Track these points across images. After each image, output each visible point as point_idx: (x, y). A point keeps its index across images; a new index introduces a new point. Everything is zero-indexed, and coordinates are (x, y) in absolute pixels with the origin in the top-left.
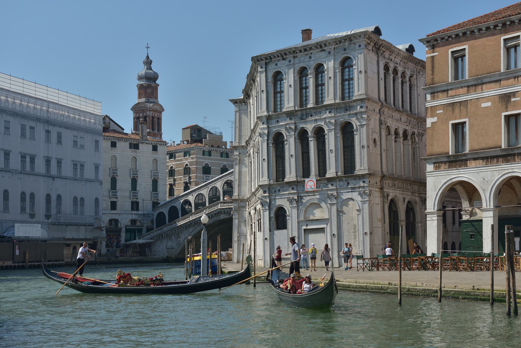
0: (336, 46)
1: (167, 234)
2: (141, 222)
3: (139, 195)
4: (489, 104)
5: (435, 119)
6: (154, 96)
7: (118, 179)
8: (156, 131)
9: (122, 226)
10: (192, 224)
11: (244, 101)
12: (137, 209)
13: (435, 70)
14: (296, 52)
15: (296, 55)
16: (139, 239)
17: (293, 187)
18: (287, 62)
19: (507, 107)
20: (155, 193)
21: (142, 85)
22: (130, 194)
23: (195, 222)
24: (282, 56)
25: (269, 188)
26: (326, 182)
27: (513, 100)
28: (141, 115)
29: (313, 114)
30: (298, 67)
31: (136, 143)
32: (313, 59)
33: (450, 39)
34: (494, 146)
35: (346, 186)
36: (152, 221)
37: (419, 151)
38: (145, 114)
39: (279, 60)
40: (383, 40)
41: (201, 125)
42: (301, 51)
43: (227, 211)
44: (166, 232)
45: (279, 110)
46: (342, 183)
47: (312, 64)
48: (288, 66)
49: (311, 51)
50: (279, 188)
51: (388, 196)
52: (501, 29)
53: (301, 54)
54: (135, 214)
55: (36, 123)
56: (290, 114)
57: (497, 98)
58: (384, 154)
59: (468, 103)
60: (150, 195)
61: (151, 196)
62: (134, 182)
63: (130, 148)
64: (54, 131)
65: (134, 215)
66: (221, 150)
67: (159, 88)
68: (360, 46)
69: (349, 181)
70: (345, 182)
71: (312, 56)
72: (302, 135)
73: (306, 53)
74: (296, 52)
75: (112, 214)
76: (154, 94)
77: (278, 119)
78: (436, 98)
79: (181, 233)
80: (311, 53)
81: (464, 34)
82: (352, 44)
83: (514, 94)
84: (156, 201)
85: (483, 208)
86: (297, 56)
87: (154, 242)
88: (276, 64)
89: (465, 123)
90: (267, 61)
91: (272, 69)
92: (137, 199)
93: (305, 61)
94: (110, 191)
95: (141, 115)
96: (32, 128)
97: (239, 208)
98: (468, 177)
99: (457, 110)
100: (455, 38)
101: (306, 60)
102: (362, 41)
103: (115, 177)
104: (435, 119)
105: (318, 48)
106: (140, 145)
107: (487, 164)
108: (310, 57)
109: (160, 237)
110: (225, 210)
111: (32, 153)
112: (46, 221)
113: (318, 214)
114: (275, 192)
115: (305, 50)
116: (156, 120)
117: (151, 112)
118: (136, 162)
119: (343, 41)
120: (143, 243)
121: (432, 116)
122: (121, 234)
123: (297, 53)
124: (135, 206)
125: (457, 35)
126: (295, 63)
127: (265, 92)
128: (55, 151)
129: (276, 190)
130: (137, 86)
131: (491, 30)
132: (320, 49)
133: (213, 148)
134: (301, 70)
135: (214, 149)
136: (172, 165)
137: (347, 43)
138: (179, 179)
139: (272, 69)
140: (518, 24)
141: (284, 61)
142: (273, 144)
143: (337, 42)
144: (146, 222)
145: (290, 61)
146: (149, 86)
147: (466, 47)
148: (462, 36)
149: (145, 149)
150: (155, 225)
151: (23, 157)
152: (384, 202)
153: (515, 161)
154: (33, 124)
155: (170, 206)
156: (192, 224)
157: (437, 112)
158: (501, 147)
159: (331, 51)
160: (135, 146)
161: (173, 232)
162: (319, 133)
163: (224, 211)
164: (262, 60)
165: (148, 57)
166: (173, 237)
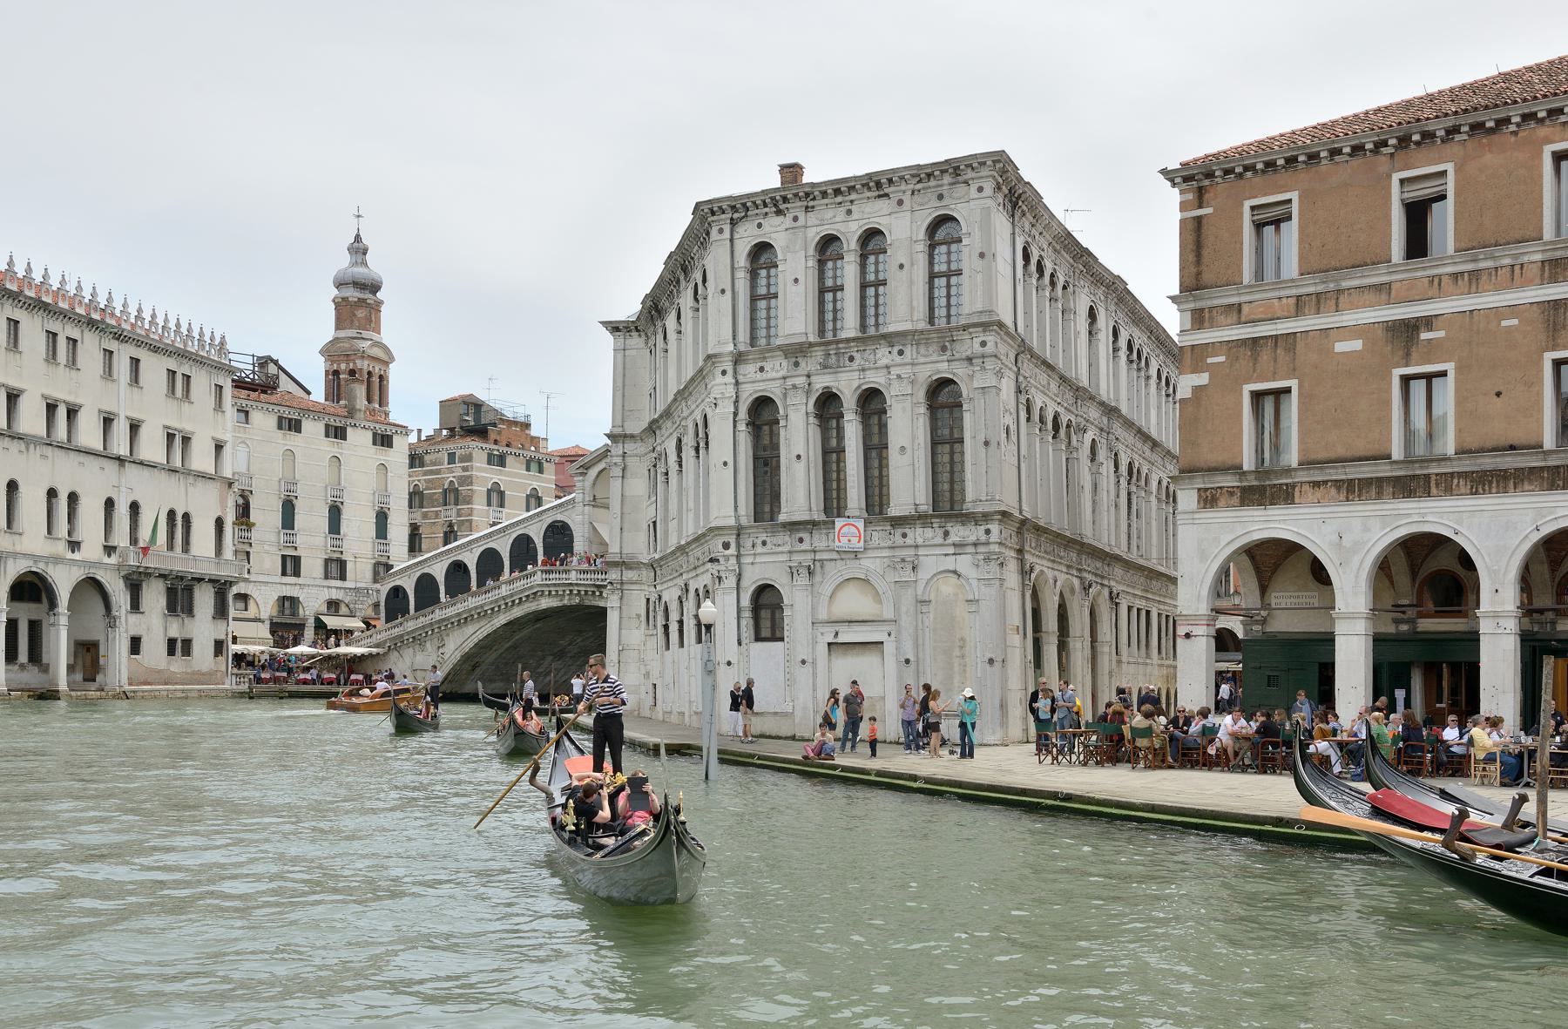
0: (919, 186)
1: (414, 638)
2: (351, 606)
3: (346, 545)
4: (1357, 345)
5: (1203, 379)
6: (373, 325)
7: (298, 504)
8: (377, 406)
9: (307, 613)
10: (472, 616)
11: (636, 327)
12: (343, 577)
13: (1205, 252)
14: (811, 197)
15: (811, 204)
16: (347, 645)
17: (801, 535)
18: (787, 221)
19: (1408, 355)
20: (382, 541)
21: (345, 299)
22: (326, 543)
23: (479, 613)
24: (775, 205)
25: (738, 535)
26: (889, 528)
27: (1424, 336)
28: (343, 366)
29: (855, 354)
30: (814, 235)
31: (339, 425)
32: (855, 216)
33: (1249, 174)
34: (1369, 454)
35: (939, 540)
36: (376, 605)
37: (1079, 468)
38: (351, 365)
39: (766, 214)
40: (1028, 183)
41: (482, 396)
42: (824, 194)
43: (557, 591)
44: (412, 631)
45: (763, 342)
46: (929, 532)
47: (850, 232)
48: (792, 231)
49: (853, 196)
50: (764, 538)
51: (1032, 570)
52: (1392, 154)
53: (826, 201)
54: (337, 588)
55: (82, 331)
56: (796, 352)
57: (1380, 332)
58: (1023, 466)
59: (1298, 340)
60: (370, 546)
61: (374, 547)
62: (335, 513)
63: (327, 435)
64: (123, 353)
65: (334, 590)
66: (528, 454)
67: (383, 308)
68: (980, 189)
69: (949, 529)
70: (937, 530)
71: (853, 208)
72: (827, 404)
73: (839, 199)
74: (811, 197)
75: (285, 584)
76: (371, 321)
77: (763, 364)
78: (1206, 324)
79: (448, 635)
80: (852, 202)
81: (1291, 161)
82: (958, 183)
83: (1428, 322)
84: (383, 560)
85: (1337, 610)
86: (813, 207)
87: (385, 654)
88: (760, 226)
89: (1288, 390)
90: (736, 216)
91: (748, 235)
92: (342, 552)
93: (833, 221)
94: (279, 532)
95: (343, 366)
96: (73, 342)
97: (622, 583)
98: (1295, 530)
99: (1265, 355)
100: (1263, 171)
101: (838, 219)
102: (987, 177)
103: (291, 501)
104: (1203, 379)
105: (869, 189)
106: (349, 430)
107: (1351, 498)
108: (849, 212)
109: (397, 644)
110: (551, 589)
111: (71, 399)
112: (106, 560)
113: (853, 602)
114: (753, 546)
115: (837, 192)
116: (376, 380)
117: (366, 363)
118: (340, 470)
119: (937, 173)
120: (363, 655)
121: (1196, 370)
122: (306, 632)
123: (814, 199)
124: (336, 567)
125: (1270, 165)
126: (809, 224)
127: (729, 293)
128: (125, 404)
129: (756, 541)
130: (334, 301)
131: (1365, 154)
132: (877, 193)
133: (509, 450)
134: (822, 242)
135: (513, 451)
136: (451, 479)
137: (947, 179)
138: (433, 515)
139: (748, 235)
140: (1443, 141)
141: (781, 218)
142: (747, 425)
143: (923, 176)
144: (360, 606)
145: (795, 219)
146: (362, 302)
147: (1294, 196)
148: (1284, 167)
149: (359, 439)
150: (383, 615)
151: (51, 408)
152: (1023, 584)
153: (1429, 493)
154: (75, 333)
155: (418, 574)
156: (472, 616)
157: (1210, 360)
158: (1389, 457)
159: (903, 198)
160: (338, 433)
161: (427, 633)
162: (871, 401)
163: (550, 592)
164: (724, 213)
165: (358, 238)
166: (428, 645)
